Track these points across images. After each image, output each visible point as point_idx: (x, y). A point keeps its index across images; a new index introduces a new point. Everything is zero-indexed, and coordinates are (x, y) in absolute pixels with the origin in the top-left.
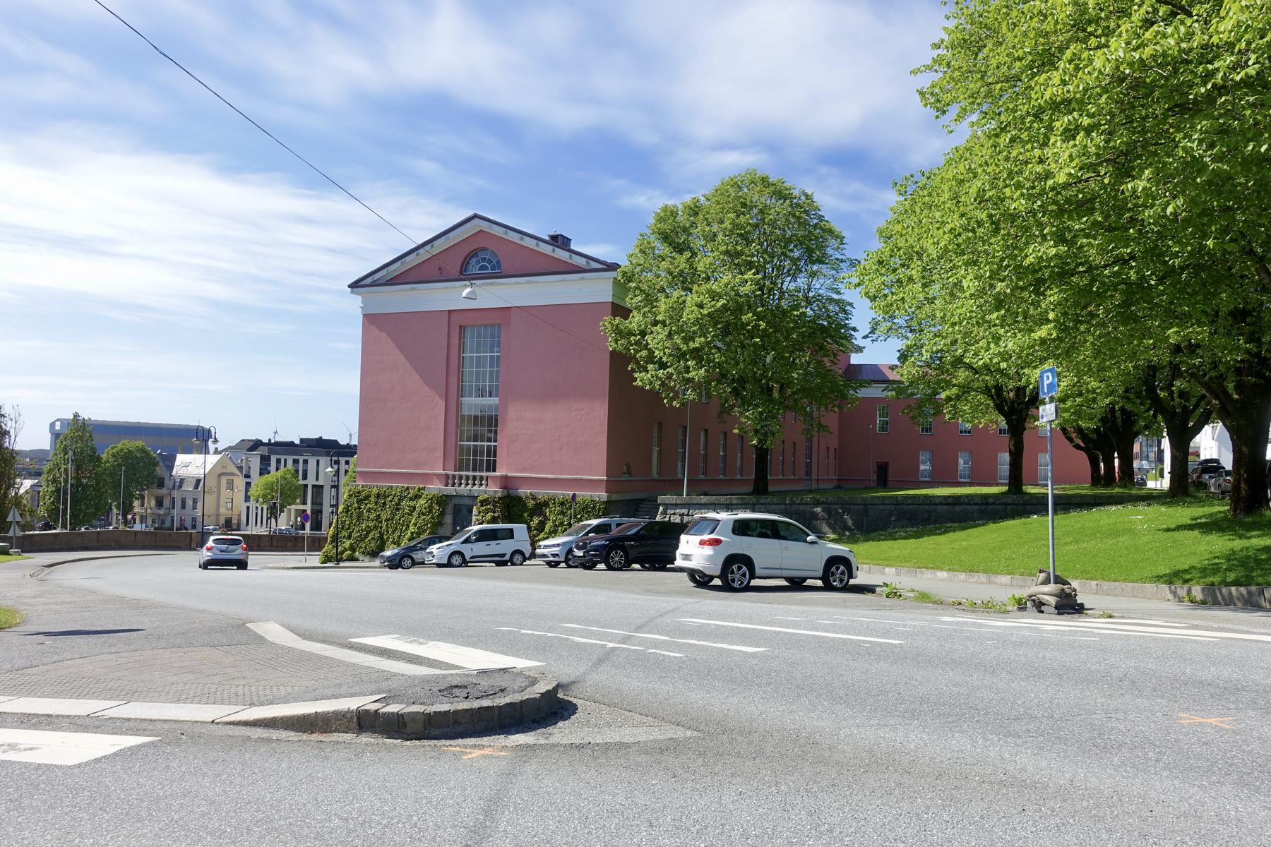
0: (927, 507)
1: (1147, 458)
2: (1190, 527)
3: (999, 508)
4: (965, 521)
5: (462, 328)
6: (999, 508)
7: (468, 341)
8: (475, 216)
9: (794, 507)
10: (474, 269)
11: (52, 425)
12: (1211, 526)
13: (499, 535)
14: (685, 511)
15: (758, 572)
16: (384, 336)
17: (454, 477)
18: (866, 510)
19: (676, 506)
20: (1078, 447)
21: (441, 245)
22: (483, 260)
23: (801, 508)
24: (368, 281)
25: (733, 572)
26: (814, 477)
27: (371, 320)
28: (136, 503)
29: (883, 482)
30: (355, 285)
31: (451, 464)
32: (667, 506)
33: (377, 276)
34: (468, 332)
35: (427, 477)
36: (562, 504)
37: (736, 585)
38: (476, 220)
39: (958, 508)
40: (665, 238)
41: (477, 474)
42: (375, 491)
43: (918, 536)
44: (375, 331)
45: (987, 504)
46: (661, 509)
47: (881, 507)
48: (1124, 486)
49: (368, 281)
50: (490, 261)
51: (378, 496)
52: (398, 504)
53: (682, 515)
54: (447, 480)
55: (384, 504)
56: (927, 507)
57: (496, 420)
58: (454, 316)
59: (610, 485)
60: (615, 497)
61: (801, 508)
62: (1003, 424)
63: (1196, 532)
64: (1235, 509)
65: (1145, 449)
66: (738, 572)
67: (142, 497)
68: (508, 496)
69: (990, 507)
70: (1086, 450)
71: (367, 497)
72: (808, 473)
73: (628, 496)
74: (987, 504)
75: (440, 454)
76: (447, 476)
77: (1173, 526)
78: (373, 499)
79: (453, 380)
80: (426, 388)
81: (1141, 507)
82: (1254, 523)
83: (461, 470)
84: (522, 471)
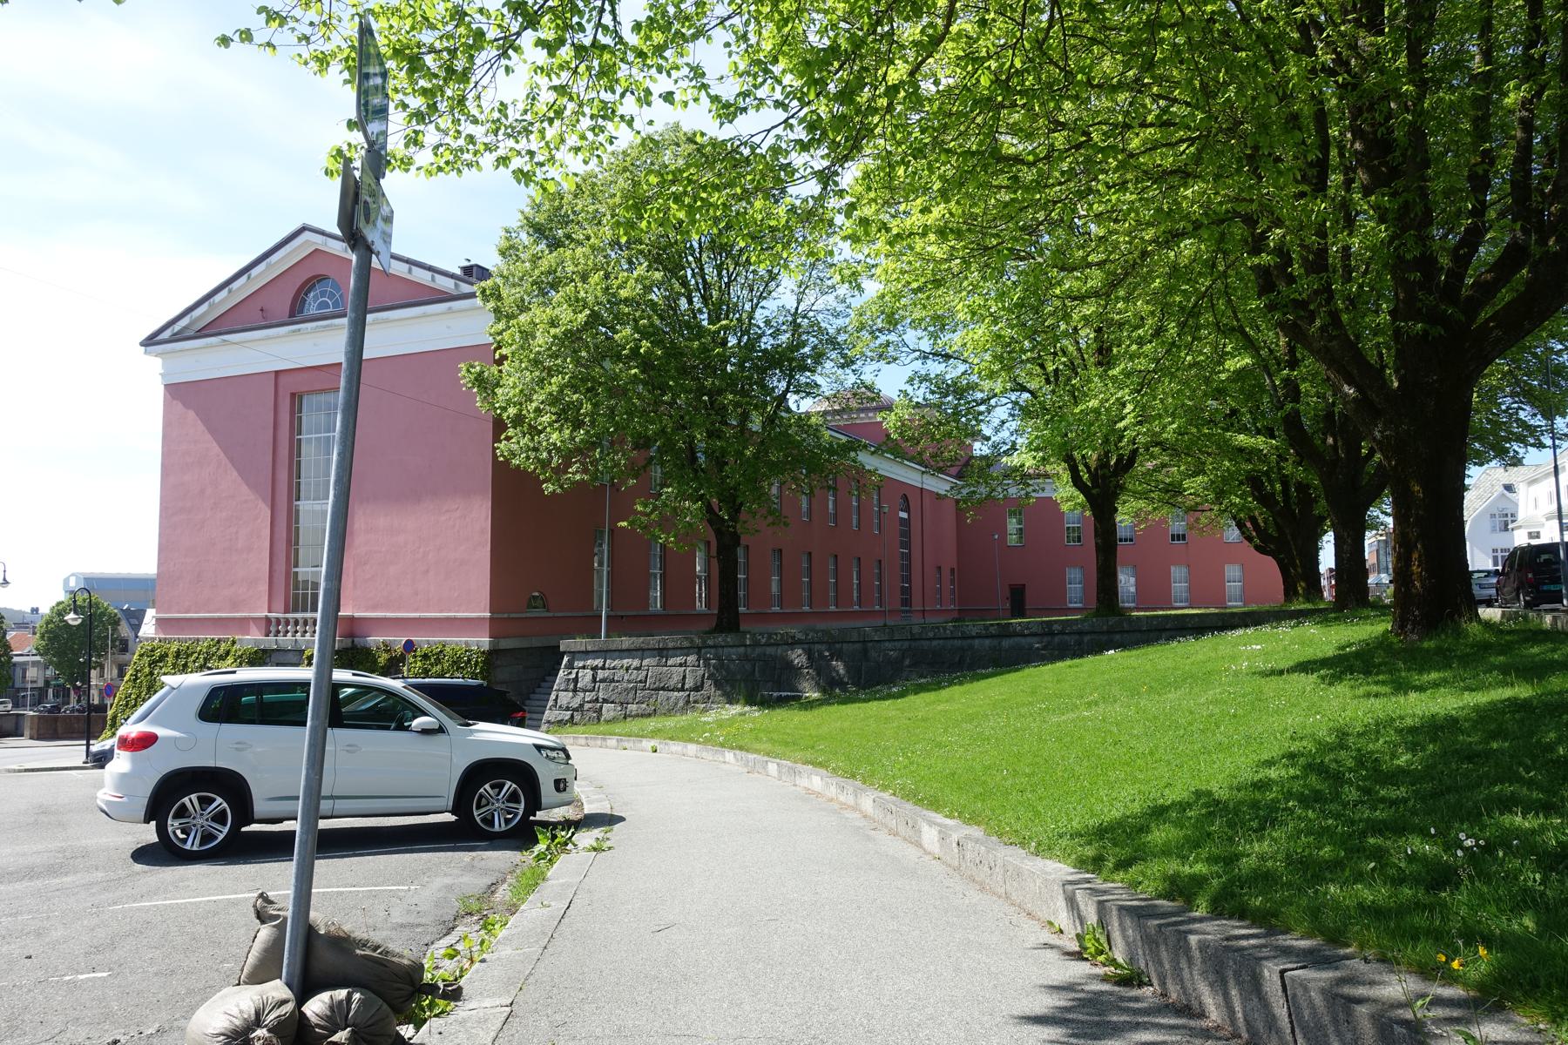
0: (958, 643)
2: (1305, 667)
3: (1071, 640)
4: (971, 667)
5: (296, 399)
6: (1071, 640)
7: (307, 419)
9: (758, 650)
10: (312, 309)
11: (66, 581)
12: (1341, 666)
14: (599, 662)
15: (260, 807)
16: (191, 414)
17: (278, 621)
18: (865, 651)
19: (586, 654)
21: (262, 275)
22: (323, 294)
23: (770, 650)
24: (166, 335)
25: (206, 802)
26: (917, 607)
27: (176, 392)
28: (94, 673)
29: (1018, 609)
30: (150, 341)
31: (280, 603)
32: (574, 655)
33: (177, 327)
35: (243, 624)
36: (425, 657)
37: (192, 845)
38: (307, 235)
39: (1006, 643)
40: (538, 230)
41: (299, 615)
42: (174, 648)
43: (938, 686)
44: (178, 407)
46: (566, 659)
48: (1308, 600)
49: (166, 335)
50: (331, 296)
51: (178, 654)
53: (594, 669)
54: (268, 625)
56: (958, 643)
58: (283, 379)
59: (496, 625)
60: (505, 644)
61: (770, 650)
63: (1313, 677)
64: (1401, 625)
66: (201, 816)
67: (102, 667)
68: (354, 647)
69: (1057, 639)
71: (163, 657)
72: (907, 602)
73: (524, 644)
74: (1052, 634)
75: (264, 587)
76: (268, 620)
77: (1285, 664)
78: (170, 660)
79: (283, 475)
80: (244, 488)
82: (1439, 651)
83: (295, 610)
84: (374, 608)
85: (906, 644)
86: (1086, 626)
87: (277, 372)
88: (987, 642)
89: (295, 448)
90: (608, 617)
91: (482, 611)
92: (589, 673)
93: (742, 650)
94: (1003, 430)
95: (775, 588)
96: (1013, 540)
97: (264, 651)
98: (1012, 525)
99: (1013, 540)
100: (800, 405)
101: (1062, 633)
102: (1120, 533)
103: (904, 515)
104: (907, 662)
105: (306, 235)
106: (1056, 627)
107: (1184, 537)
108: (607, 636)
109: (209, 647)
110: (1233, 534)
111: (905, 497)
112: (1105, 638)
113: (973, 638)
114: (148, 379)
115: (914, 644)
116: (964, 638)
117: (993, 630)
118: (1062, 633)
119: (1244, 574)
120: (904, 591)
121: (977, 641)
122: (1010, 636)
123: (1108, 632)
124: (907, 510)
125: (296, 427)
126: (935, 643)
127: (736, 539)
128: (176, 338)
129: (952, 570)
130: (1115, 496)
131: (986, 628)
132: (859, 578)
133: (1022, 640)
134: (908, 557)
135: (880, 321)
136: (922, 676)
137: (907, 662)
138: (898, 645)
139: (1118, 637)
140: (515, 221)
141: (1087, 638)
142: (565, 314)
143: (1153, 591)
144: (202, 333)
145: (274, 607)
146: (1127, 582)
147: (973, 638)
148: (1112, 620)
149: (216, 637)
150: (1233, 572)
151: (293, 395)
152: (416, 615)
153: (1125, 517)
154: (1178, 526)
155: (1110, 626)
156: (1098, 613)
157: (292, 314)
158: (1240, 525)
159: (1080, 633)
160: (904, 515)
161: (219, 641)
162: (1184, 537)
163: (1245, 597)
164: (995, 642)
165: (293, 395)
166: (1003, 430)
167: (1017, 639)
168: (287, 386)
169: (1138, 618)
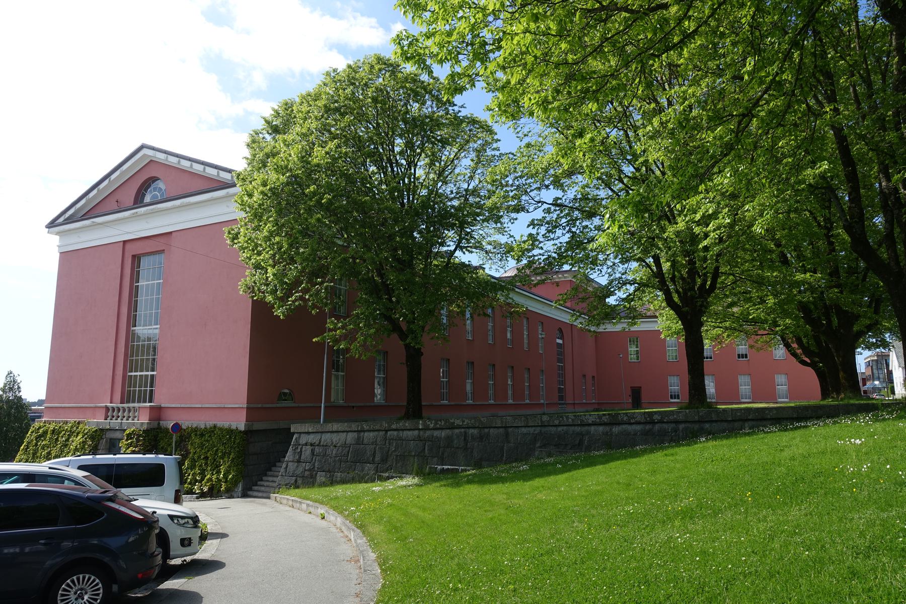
1: (879, 379)
3: (669, 427)
5: (136, 259)
6: (669, 427)
8: (142, 147)
9: (428, 433)
10: (147, 199)
13: (37, 479)
20: (804, 363)
24: (61, 220)
27: (67, 258)
30: (52, 225)
34: (144, 262)
36: (202, 435)
39: (616, 429)
41: (131, 405)
42: (52, 427)
45: (653, 422)
47: (524, 430)
49: (61, 220)
51: (53, 431)
52: (67, 440)
55: (57, 440)
56: (578, 429)
57: (154, 348)
59: (252, 411)
60: (257, 426)
62: (680, 325)
65: (875, 371)
69: (657, 427)
70: (813, 365)
72: (561, 398)
74: (653, 422)
76: (107, 409)
81: (862, 421)
83: (128, 402)
85: (538, 429)
86: (681, 417)
87: (125, 242)
88: (601, 428)
89: (134, 292)
90: (325, 407)
91: (241, 400)
92: (309, 448)
93: (416, 432)
94: (615, 274)
95: (469, 388)
96: (632, 358)
97: (102, 430)
98: (633, 349)
99: (632, 358)
100: (315, 161)
101: (661, 422)
102: (705, 354)
103: (559, 341)
104: (538, 445)
105: (145, 151)
106: (656, 417)
107: (746, 355)
108: (324, 422)
109: (72, 427)
110: (780, 352)
111: (560, 330)
112: (696, 427)
113: (589, 425)
114: (48, 251)
115: (544, 429)
116: (582, 425)
117: (605, 419)
118: (661, 422)
119: (789, 379)
120: (560, 390)
121: (593, 428)
122: (619, 424)
123: (699, 422)
124: (562, 338)
125: (135, 276)
126: (560, 429)
127: (419, 353)
128: (69, 221)
129: (593, 377)
130: (701, 313)
131: (600, 417)
132: (513, 381)
133: (629, 428)
134: (563, 368)
135: (528, 198)
136: (550, 455)
137: (538, 445)
138: (531, 430)
139: (707, 426)
140: (260, 125)
141: (681, 426)
142: (273, 176)
143: (730, 391)
144: (85, 217)
145: (115, 399)
146: (710, 387)
147: (589, 425)
148: (703, 411)
149: (78, 420)
150: (781, 379)
151: (134, 256)
152: (362, 404)
153: (712, 335)
154: (742, 349)
155: (702, 419)
156: (690, 406)
157: (135, 202)
158: (787, 346)
159: (677, 422)
160: (559, 341)
161: (79, 423)
162: (746, 355)
163: (791, 395)
164: (607, 428)
165: (134, 256)
166: (615, 274)
167: (624, 426)
168: (132, 250)
169: (724, 410)
